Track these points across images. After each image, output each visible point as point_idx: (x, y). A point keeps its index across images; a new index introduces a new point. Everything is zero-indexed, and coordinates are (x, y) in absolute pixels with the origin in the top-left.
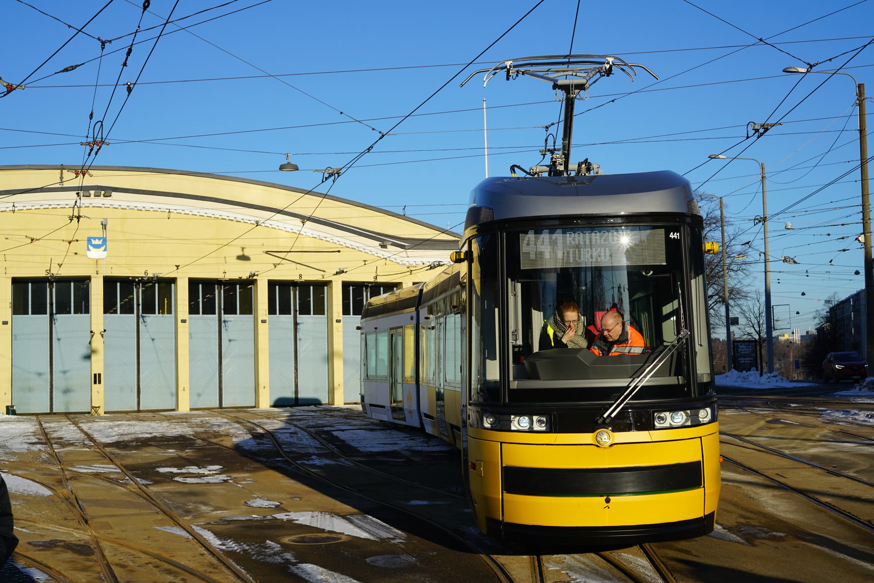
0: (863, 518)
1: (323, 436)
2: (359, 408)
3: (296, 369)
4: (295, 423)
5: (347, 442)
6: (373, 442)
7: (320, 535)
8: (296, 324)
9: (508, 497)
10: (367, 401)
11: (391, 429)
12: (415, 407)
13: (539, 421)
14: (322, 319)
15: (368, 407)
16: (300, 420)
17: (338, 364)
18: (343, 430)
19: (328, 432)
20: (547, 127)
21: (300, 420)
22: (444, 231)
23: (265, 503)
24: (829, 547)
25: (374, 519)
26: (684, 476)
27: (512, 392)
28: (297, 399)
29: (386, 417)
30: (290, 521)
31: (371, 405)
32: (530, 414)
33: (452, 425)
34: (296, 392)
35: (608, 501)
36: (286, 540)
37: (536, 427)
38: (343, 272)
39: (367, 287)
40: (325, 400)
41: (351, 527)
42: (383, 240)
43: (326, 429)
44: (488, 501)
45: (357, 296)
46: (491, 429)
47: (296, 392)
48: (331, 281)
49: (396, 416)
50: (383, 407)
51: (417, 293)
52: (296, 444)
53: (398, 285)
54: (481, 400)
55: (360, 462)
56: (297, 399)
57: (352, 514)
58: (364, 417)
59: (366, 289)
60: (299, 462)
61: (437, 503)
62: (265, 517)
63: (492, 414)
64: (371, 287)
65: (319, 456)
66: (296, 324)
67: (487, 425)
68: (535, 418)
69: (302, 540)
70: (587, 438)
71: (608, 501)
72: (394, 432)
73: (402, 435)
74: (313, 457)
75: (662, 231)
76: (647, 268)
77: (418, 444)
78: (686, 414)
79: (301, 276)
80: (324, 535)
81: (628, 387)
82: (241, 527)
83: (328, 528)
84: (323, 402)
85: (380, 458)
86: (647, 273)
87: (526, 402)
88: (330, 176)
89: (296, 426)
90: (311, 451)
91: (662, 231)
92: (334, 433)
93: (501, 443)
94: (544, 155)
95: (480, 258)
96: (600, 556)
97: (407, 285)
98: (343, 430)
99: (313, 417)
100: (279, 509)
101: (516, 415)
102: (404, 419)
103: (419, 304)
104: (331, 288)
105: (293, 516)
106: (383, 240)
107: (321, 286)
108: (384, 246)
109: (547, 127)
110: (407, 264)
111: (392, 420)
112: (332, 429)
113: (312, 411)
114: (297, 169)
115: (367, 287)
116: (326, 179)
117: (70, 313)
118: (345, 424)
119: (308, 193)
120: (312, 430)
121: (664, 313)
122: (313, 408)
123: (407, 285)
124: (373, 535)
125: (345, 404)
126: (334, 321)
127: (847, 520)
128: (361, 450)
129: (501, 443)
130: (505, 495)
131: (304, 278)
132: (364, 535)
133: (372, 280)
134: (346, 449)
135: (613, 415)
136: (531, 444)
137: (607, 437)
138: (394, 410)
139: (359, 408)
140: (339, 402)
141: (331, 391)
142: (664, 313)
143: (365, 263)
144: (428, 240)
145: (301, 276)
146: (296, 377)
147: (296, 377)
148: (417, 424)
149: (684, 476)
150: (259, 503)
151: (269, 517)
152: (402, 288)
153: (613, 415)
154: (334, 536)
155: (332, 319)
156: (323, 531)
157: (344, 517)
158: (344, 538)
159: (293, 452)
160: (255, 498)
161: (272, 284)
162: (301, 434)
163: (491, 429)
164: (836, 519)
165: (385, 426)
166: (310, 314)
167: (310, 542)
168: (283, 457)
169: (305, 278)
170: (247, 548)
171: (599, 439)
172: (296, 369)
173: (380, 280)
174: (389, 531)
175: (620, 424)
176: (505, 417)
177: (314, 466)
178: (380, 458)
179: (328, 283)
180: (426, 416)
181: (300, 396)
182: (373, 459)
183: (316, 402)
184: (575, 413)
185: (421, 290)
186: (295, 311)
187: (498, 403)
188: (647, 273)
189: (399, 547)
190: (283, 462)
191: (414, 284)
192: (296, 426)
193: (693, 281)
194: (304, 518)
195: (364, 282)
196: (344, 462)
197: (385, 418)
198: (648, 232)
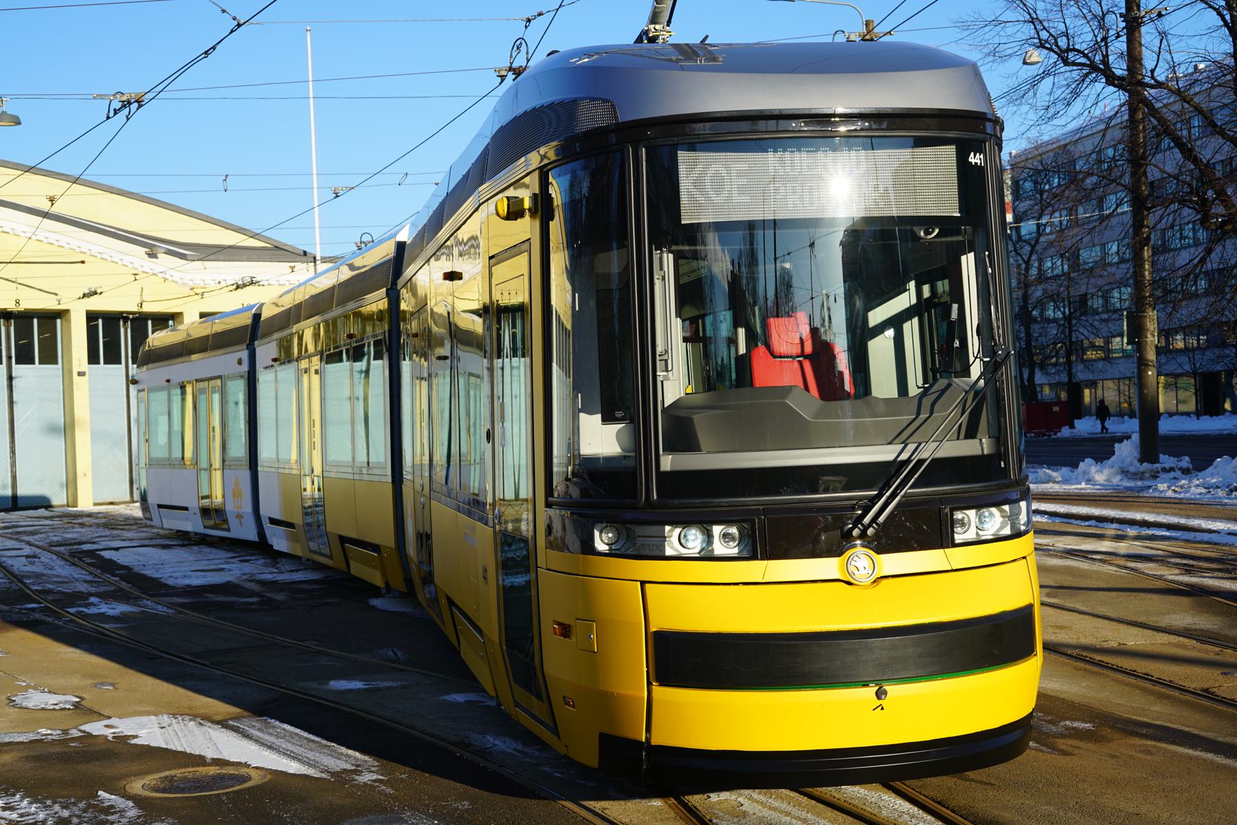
0: (1192, 686)
1: (88, 560)
2: (136, 511)
3: (13, 452)
4: (26, 538)
5: (136, 569)
6: (183, 569)
7: (202, 770)
8: (10, 378)
9: (663, 693)
10: (153, 500)
11: (198, 544)
12: (247, 507)
13: (725, 536)
14: (52, 372)
15: (154, 511)
16: (32, 533)
17: (83, 438)
18: (117, 549)
19: (91, 553)
20: (529, 20)
21: (32, 533)
22: (255, 236)
23: (51, 700)
24: (1216, 752)
25: (350, 752)
26: (992, 641)
27: (664, 477)
28: (15, 497)
29: (192, 524)
30: (122, 740)
31: (160, 506)
32: (704, 522)
33: (343, 540)
34: (14, 486)
35: (880, 694)
36: (137, 786)
37: (719, 548)
38: (96, 293)
39: (126, 319)
40: (59, 499)
41: (253, 747)
42: (151, 245)
43: (86, 547)
44: (607, 702)
45: (114, 334)
46: (610, 555)
47: (14, 486)
48: (67, 311)
49: (211, 523)
50: (186, 509)
51: (249, 321)
52: (48, 576)
53: (176, 317)
54: (575, 492)
55: (181, 605)
56: (15, 497)
57: (236, 718)
58: (157, 523)
59: (125, 323)
60: (72, 610)
61: (383, 684)
62: (65, 732)
63: (608, 521)
64: (132, 320)
65: (104, 596)
66: (10, 378)
67: (601, 546)
68: (717, 530)
69: (170, 785)
70: (827, 567)
71: (880, 694)
72: (206, 550)
73: (222, 554)
74: (92, 599)
75: (951, 150)
76: (929, 222)
77: (234, 570)
78: (1002, 511)
79: (18, 302)
80: (213, 770)
81: (909, 461)
82: (28, 758)
83: (210, 754)
84: (55, 502)
85: (212, 597)
86: (927, 233)
87: (699, 499)
88: (124, 106)
89: (29, 543)
90: (83, 588)
91: (951, 150)
92: (102, 553)
93: (643, 583)
94: (503, 78)
95: (572, 207)
96: (801, 793)
97: (191, 317)
98: (117, 549)
99: (53, 528)
100: (82, 710)
101: (674, 523)
102: (229, 530)
103: (253, 338)
104: (69, 321)
105: (125, 726)
106: (151, 245)
107: (51, 318)
108: (152, 255)
109: (529, 20)
110: (191, 283)
111: (201, 530)
112: (95, 547)
113: (46, 518)
114: (19, 123)
115: (126, 319)
116: (116, 112)
117: (33, 363)
118: (114, 538)
119: (29, 169)
120: (62, 549)
121: (872, 323)
122: (42, 512)
123: (191, 317)
124: (310, 765)
125: (95, 504)
126: (75, 374)
127: (1164, 690)
128: (171, 582)
129: (643, 583)
130: (658, 690)
131: (23, 306)
132: (293, 767)
133: (135, 309)
134: (140, 584)
135: (881, 519)
136: (709, 584)
137: (861, 560)
138: (205, 512)
139: (136, 511)
140: (85, 503)
141: (71, 483)
142: (872, 323)
143: (129, 284)
144: (230, 247)
145: (18, 302)
146: (13, 465)
147: (13, 465)
148: (251, 535)
149: (992, 641)
150: (36, 700)
151: (75, 733)
152: (182, 322)
153: (881, 519)
154: (231, 771)
155: (71, 371)
156: (199, 760)
157: (223, 724)
158: (256, 779)
159: (50, 592)
160: (26, 689)
161: (92, 317)
162: (46, 557)
163: (610, 555)
164: (1144, 690)
165: (184, 539)
166: (33, 363)
167: (182, 790)
168: (39, 603)
169: (25, 305)
170: (66, 813)
171: (852, 569)
172: (13, 452)
173: (147, 308)
174: (339, 756)
175: (890, 539)
176: (652, 530)
177: (103, 617)
178: (212, 597)
179: (62, 314)
180: (273, 521)
181: (21, 492)
182: (199, 598)
183: (42, 503)
184: (786, 520)
185: (257, 317)
186: (9, 358)
187: (623, 504)
188: (927, 233)
189: (382, 793)
190: (44, 610)
191: (202, 315)
192: (29, 543)
193: (963, 258)
194: (149, 731)
195: (122, 313)
196: (152, 606)
197: (188, 527)
198: (906, 154)
